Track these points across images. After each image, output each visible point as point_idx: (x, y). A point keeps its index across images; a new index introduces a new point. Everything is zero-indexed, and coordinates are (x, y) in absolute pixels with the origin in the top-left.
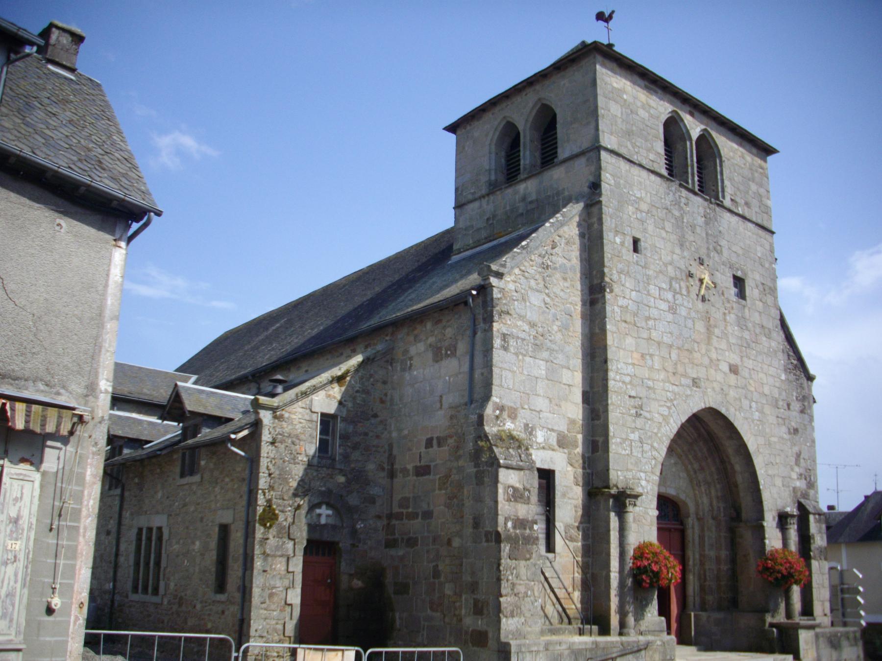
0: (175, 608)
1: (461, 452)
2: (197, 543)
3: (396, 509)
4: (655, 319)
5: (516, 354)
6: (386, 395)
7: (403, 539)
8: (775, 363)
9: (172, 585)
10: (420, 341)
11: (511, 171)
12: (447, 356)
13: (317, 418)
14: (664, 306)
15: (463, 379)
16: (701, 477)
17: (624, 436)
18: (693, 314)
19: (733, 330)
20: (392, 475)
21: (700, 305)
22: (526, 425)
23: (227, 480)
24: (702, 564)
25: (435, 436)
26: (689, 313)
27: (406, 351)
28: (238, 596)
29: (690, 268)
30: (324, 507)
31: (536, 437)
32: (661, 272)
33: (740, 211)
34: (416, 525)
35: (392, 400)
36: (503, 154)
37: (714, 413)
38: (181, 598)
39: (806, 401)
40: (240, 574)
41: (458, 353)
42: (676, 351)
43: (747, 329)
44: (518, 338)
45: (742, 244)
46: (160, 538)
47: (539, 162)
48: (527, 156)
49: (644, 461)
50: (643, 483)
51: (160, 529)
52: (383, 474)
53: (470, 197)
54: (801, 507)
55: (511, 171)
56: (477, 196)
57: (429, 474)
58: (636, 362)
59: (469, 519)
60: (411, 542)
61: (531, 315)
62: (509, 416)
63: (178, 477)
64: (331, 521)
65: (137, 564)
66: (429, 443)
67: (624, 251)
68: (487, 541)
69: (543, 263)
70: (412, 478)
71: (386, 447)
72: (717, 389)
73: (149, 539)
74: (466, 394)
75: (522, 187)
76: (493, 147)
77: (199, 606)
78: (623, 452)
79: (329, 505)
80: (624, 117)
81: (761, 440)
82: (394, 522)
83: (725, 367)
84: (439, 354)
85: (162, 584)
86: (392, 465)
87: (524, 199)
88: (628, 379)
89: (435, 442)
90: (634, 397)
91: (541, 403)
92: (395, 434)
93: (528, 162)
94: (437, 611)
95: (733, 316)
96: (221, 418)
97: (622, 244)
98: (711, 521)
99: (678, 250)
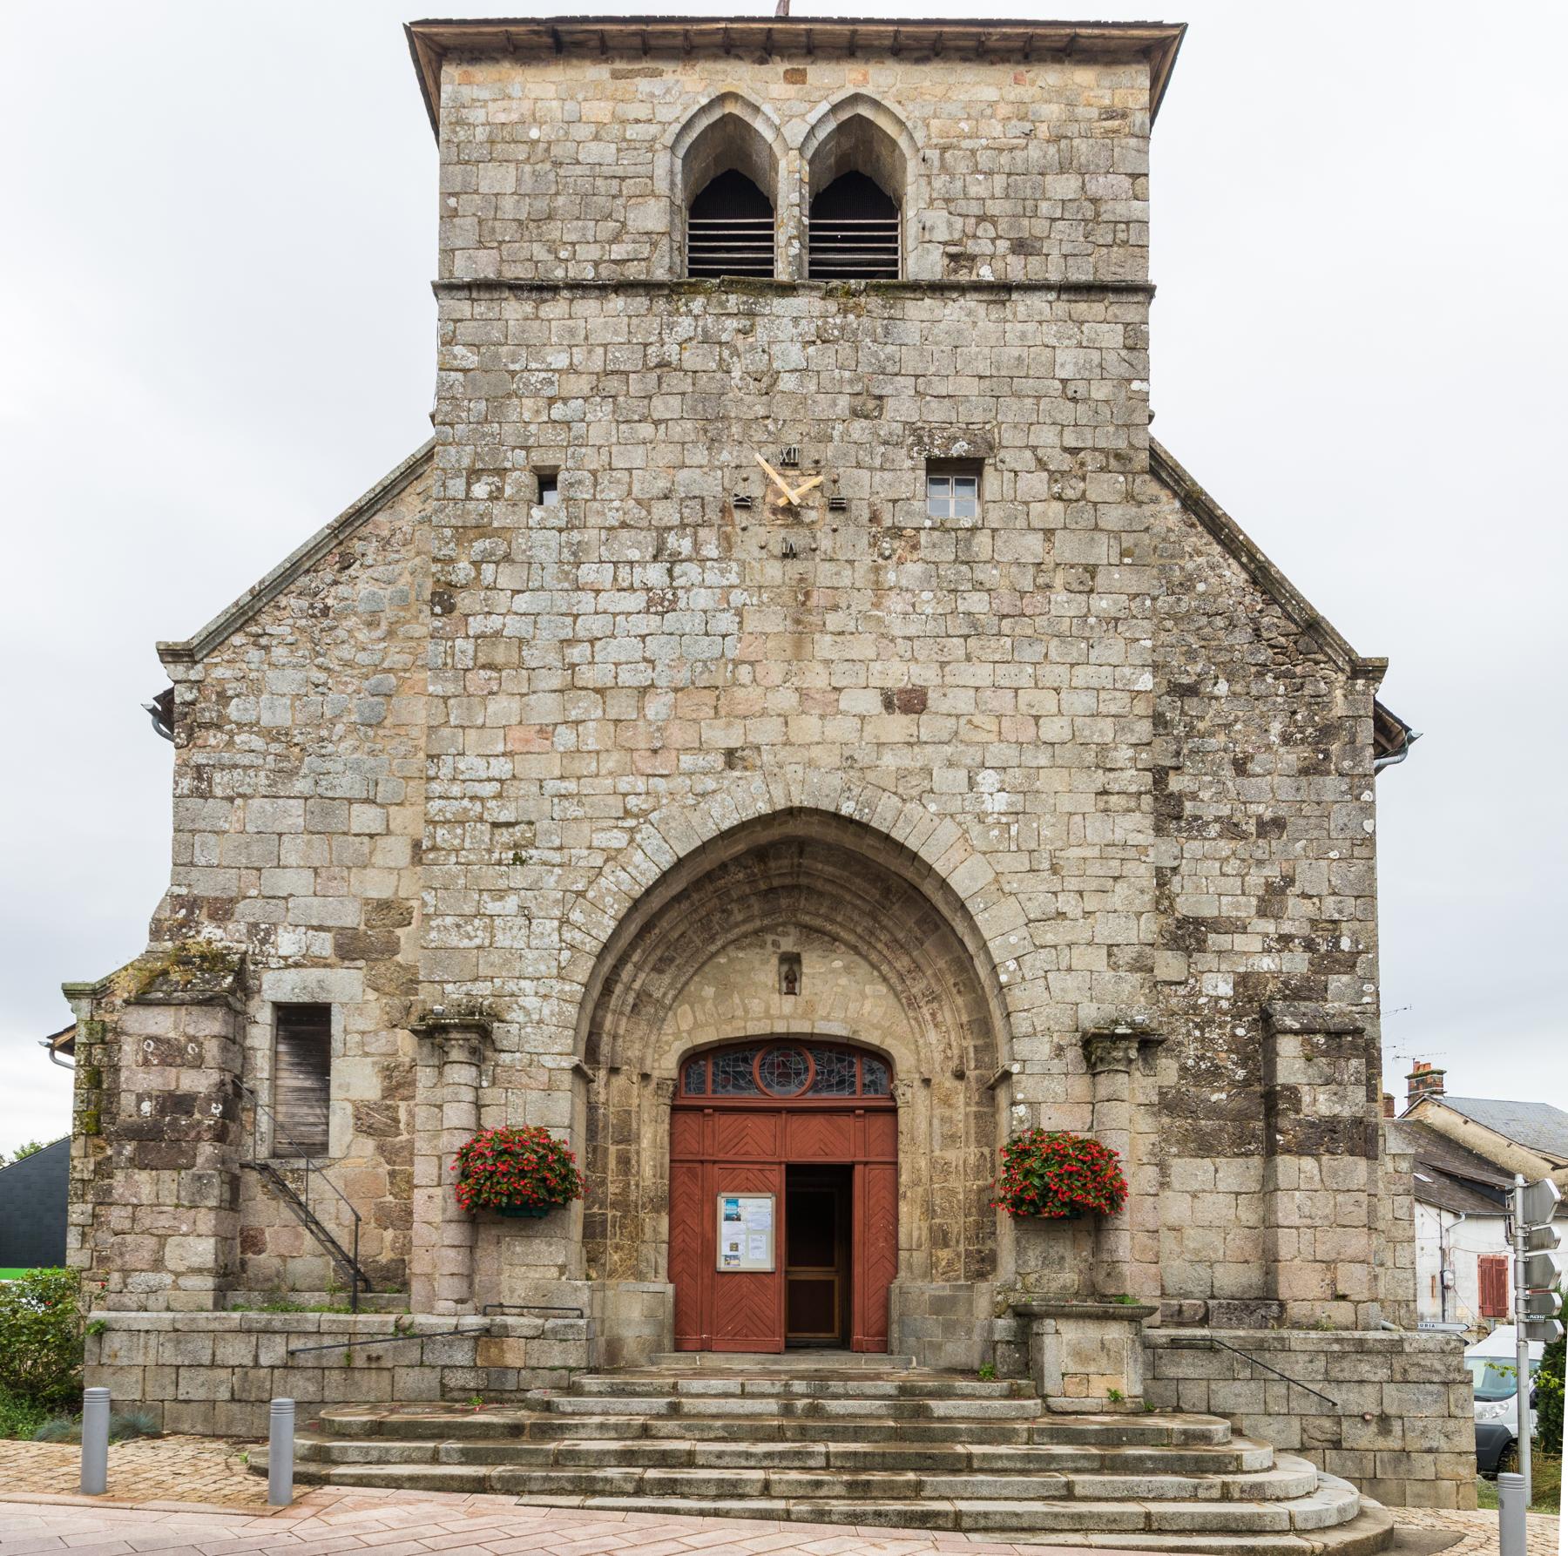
5: (231, 799)
16: (917, 988)
44: (235, 766)
49: (529, 954)
62: (211, 917)
69: (312, 606)
78: (466, 943)
91: (294, 881)
99: (699, 456)
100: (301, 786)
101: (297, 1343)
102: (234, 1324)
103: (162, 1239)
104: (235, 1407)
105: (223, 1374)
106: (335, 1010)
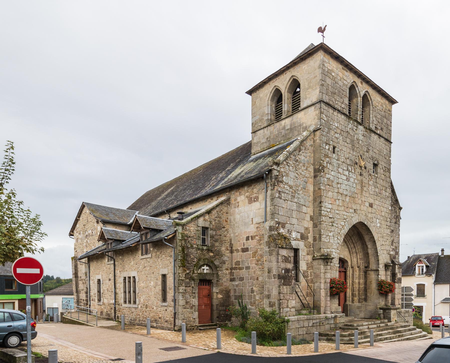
0: (144, 309)
1: (262, 242)
2: (152, 283)
3: (234, 266)
4: (341, 184)
5: (285, 200)
6: (228, 218)
7: (237, 278)
8: (388, 202)
9: (142, 300)
10: (242, 195)
11: (278, 115)
12: (255, 201)
13: (200, 229)
14: (345, 178)
15: (262, 212)
17: (327, 234)
18: (356, 181)
19: (372, 188)
20: (232, 252)
21: (359, 177)
22: (288, 230)
23: (163, 256)
24: (353, 285)
25: (250, 235)
26: (354, 181)
27: (236, 200)
28: (172, 303)
29: (356, 160)
30: (205, 266)
31: (292, 235)
32: (344, 162)
33: (378, 132)
34: (243, 273)
35: (230, 220)
36: (274, 105)
37: (361, 224)
38: (147, 305)
39: (398, 218)
40: (173, 295)
41: (259, 200)
42: (349, 198)
43: (377, 187)
44: (285, 193)
45: (378, 148)
46: (134, 281)
47: (291, 109)
48: (286, 106)
49: (334, 244)
50: (334, 253)
51: (134, 277)
52: (228, 252)
53: (259, 128)
54: (393, 262)
55: (278, 115)
56: (262, 127)
57: (248, 251)
58: (332, 203)
59: (266, 269)
60: (242, 279)
61: (291, 183)
62: (282, 227)
63: (140, 256)
64: (208, 272)
65: (125, 292)
66: (247, 239)
67: (329, 153)
68: (274, 278)
70: (241, 253)
71: (229, 240)
72: (364, 214)
73: (129, 282)
74: (264, 217)
75: (283, 122)
76: (269, 102)
77: (155, 308)
78: (327, 241)
79: (207, 265)
80: (332, 85)
81: (380, 235)
82: (233, 271)
83: (367, 204)
84: (251, 200)
85: (137, 300)
86: (232, 248)
87: (284, 128)
88: (329, 210)
89: (250, 238)
90: (331, 218)
91: (294, 221)
92: (232, 235)
93: (286, 109)
94: (253, 306)
95: (372, 182)
96: (157, 230)
97: (329, 150)
98: (357, 268)
99: (352, 152)
100: (296, 200)
101: (314, 321)
102: (306, 318)
103: (288, 300)
104: (306, 335)
105: (304, 328)
106: (300, 250)
